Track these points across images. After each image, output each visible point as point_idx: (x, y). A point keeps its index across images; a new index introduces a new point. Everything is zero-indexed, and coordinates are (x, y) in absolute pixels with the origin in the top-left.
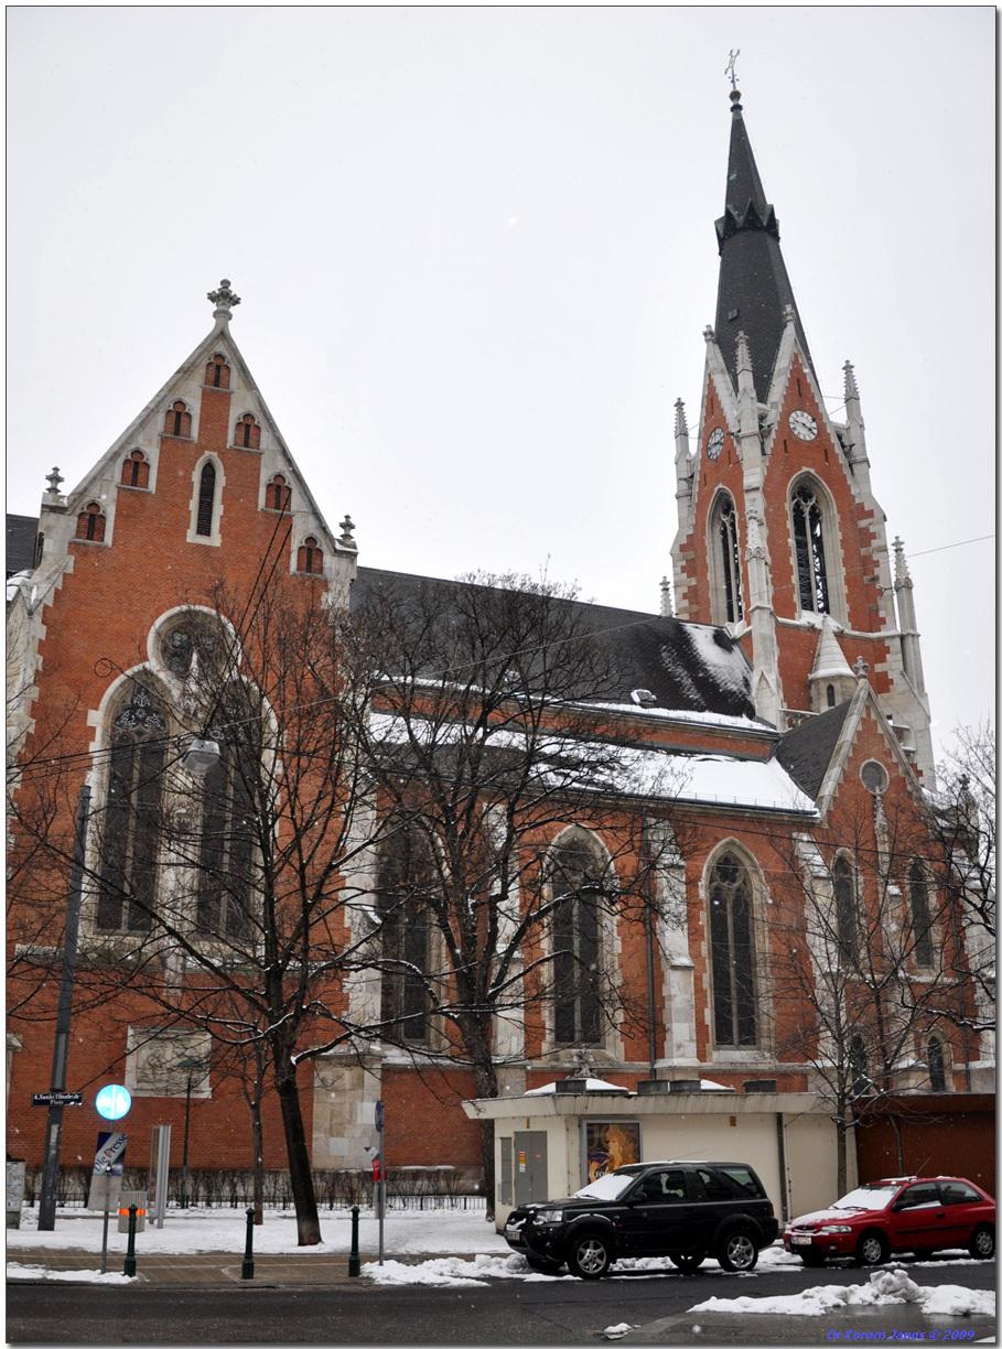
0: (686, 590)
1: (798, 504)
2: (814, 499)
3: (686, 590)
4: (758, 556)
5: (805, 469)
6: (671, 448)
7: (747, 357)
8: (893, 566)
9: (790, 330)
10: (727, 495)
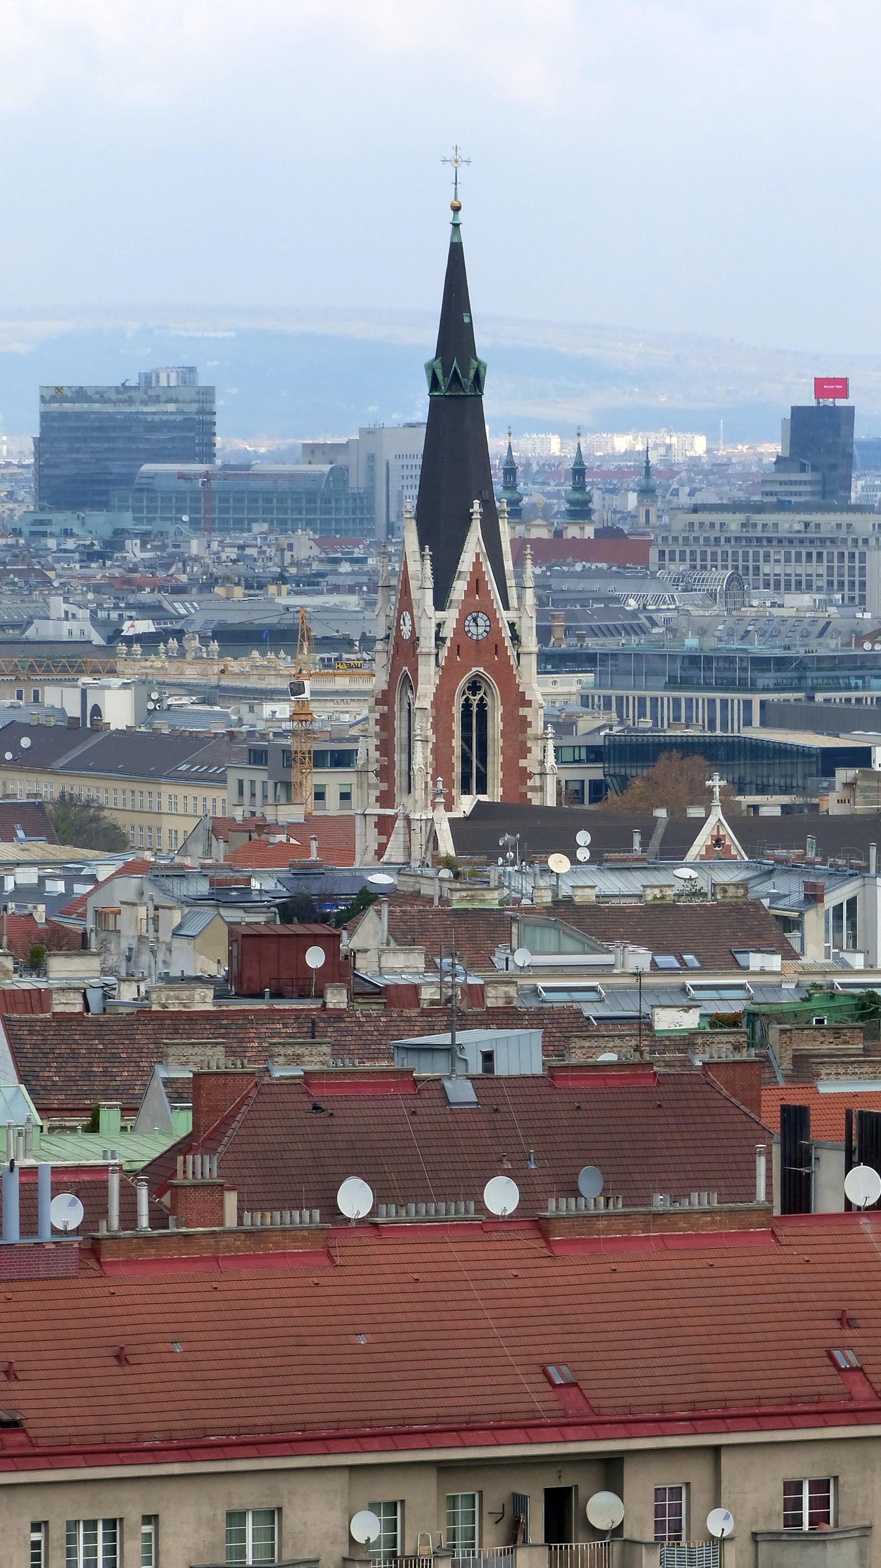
1: (467, 699)
2: (482, 692)
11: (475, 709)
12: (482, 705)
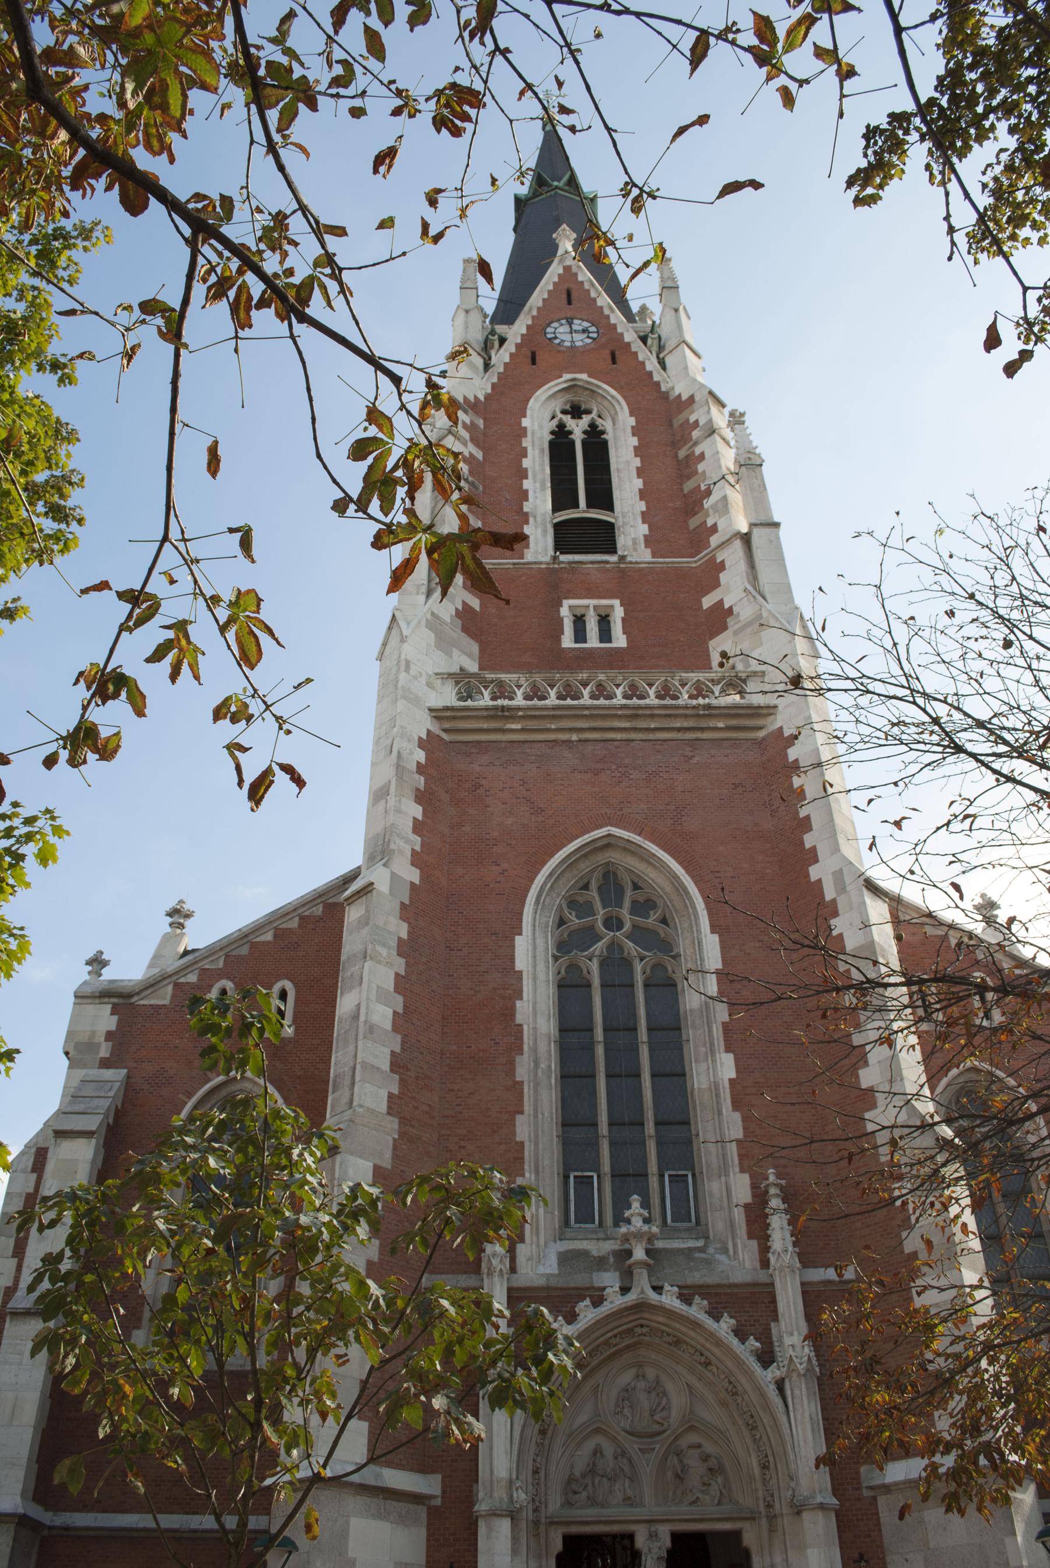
11: (578, 437)
12: (594, 433)
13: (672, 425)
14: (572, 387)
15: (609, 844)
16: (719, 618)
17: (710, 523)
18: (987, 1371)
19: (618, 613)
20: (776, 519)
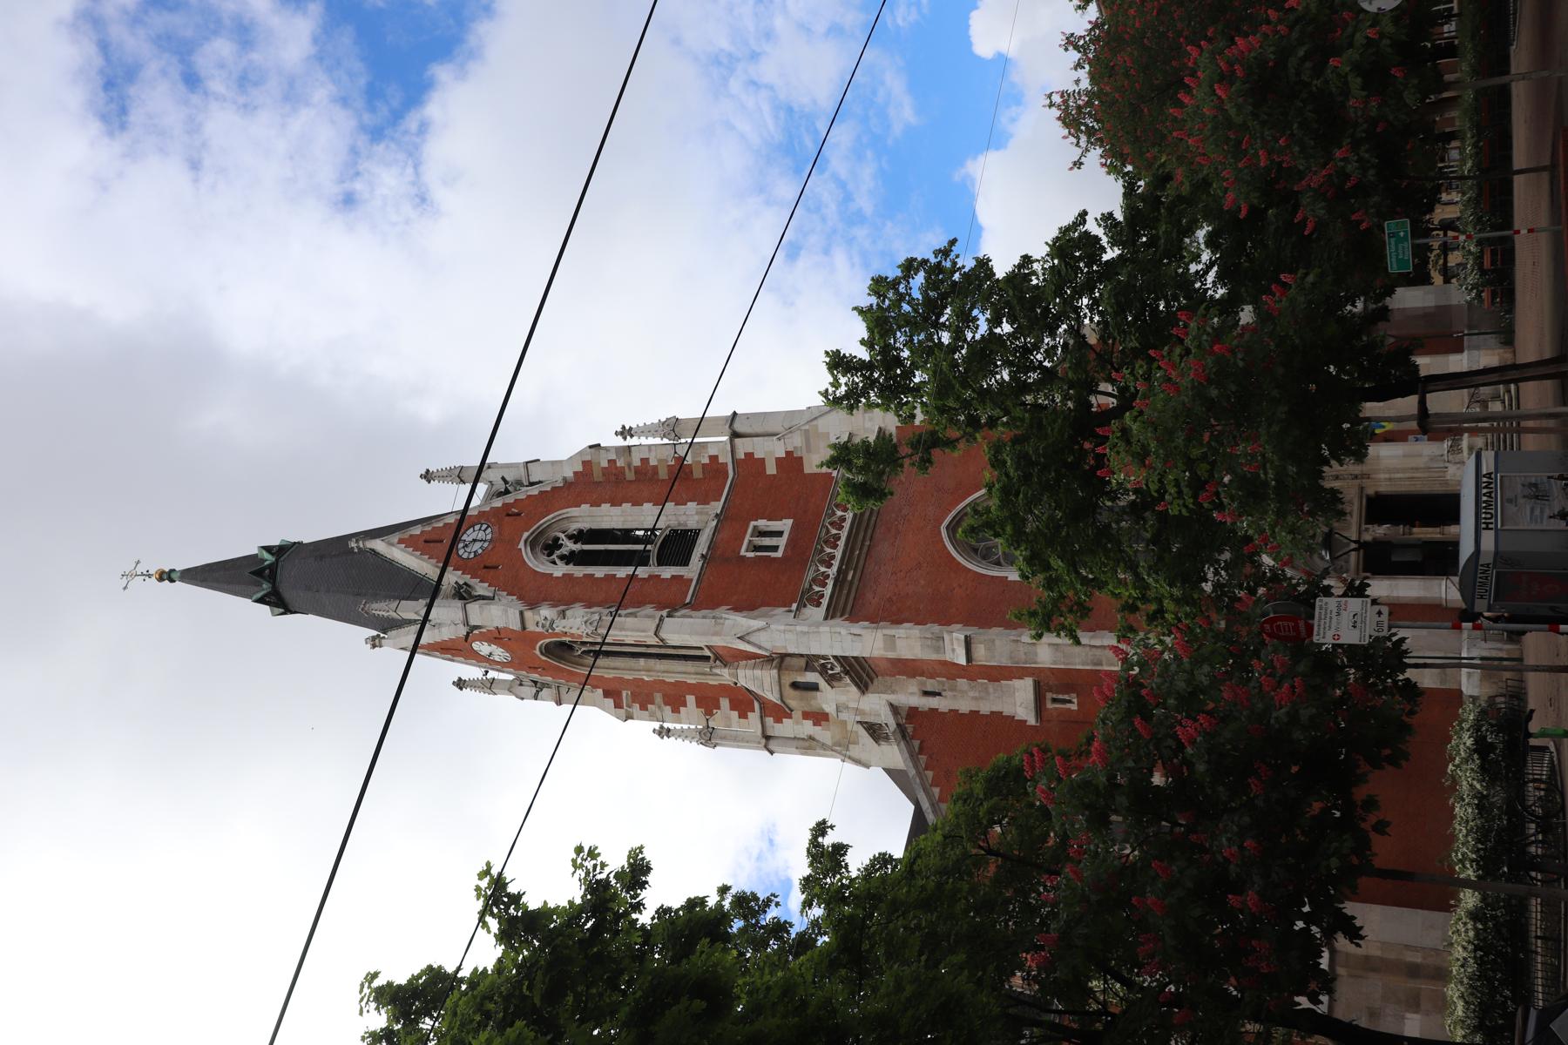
0: (735, 714)
1: (562, 558)
2: (562, 536)
3: (735, 714)
4: (891, 641)
5: (521, 545)
6: (506, 701)
7: (383, 605)
8: (644, 441)
9: (378, 545)
10: (547, 645)
11: (578, 547)
12: (579, 536)
13: (601, 476)
14: (532, 544)
15: (952, 529)
16: (791, 462)
17: (706, 461)
18: (1308, 919)
19: (762, 523)
20: (729, 413)
